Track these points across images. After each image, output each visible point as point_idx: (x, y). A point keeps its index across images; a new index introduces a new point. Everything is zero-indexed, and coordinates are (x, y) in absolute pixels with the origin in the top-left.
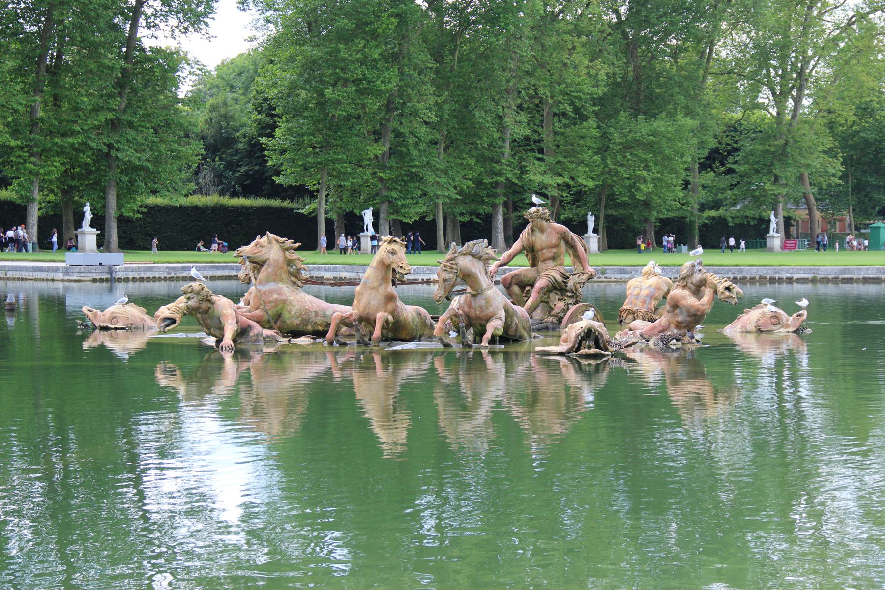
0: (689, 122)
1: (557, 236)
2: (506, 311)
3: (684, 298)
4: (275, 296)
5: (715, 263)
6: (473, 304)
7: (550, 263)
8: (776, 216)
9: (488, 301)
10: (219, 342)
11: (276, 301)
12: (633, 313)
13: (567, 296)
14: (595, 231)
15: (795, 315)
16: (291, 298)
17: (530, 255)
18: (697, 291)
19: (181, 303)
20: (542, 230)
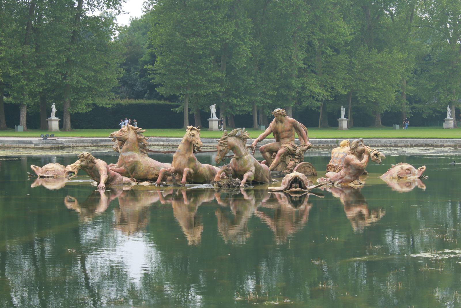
0: (401, 56)
1: (291, 125)
2: (256, 167)
3: (352, 160)
4: (131, 159)
5: (406, 136)
6: (237, 164)
7: (288, 140)
8: (450, 108)
9: (246, 162)
10: (98, 184)
11: (132, 161)
12: (334, 167)
13: (295, 158)
14: (345, 116)
15: (419, 169)
16: (140, 160)
17: (275, 135)
18: (360, 156)
19: (78, 163)
20: (282, 122)
